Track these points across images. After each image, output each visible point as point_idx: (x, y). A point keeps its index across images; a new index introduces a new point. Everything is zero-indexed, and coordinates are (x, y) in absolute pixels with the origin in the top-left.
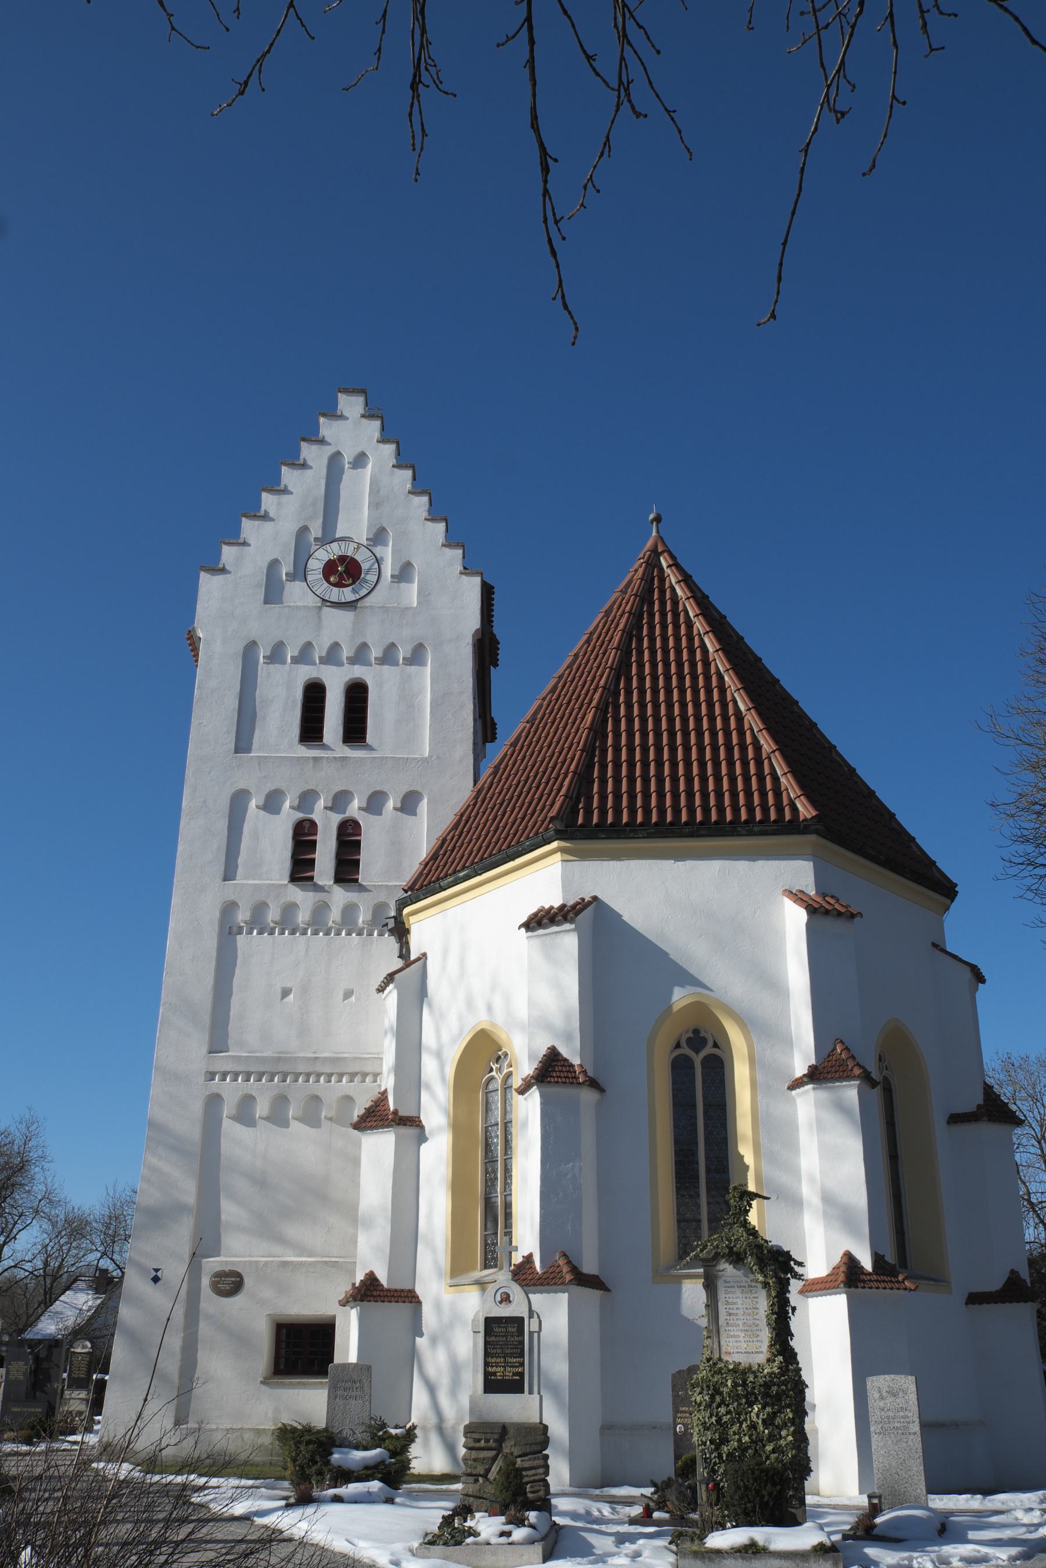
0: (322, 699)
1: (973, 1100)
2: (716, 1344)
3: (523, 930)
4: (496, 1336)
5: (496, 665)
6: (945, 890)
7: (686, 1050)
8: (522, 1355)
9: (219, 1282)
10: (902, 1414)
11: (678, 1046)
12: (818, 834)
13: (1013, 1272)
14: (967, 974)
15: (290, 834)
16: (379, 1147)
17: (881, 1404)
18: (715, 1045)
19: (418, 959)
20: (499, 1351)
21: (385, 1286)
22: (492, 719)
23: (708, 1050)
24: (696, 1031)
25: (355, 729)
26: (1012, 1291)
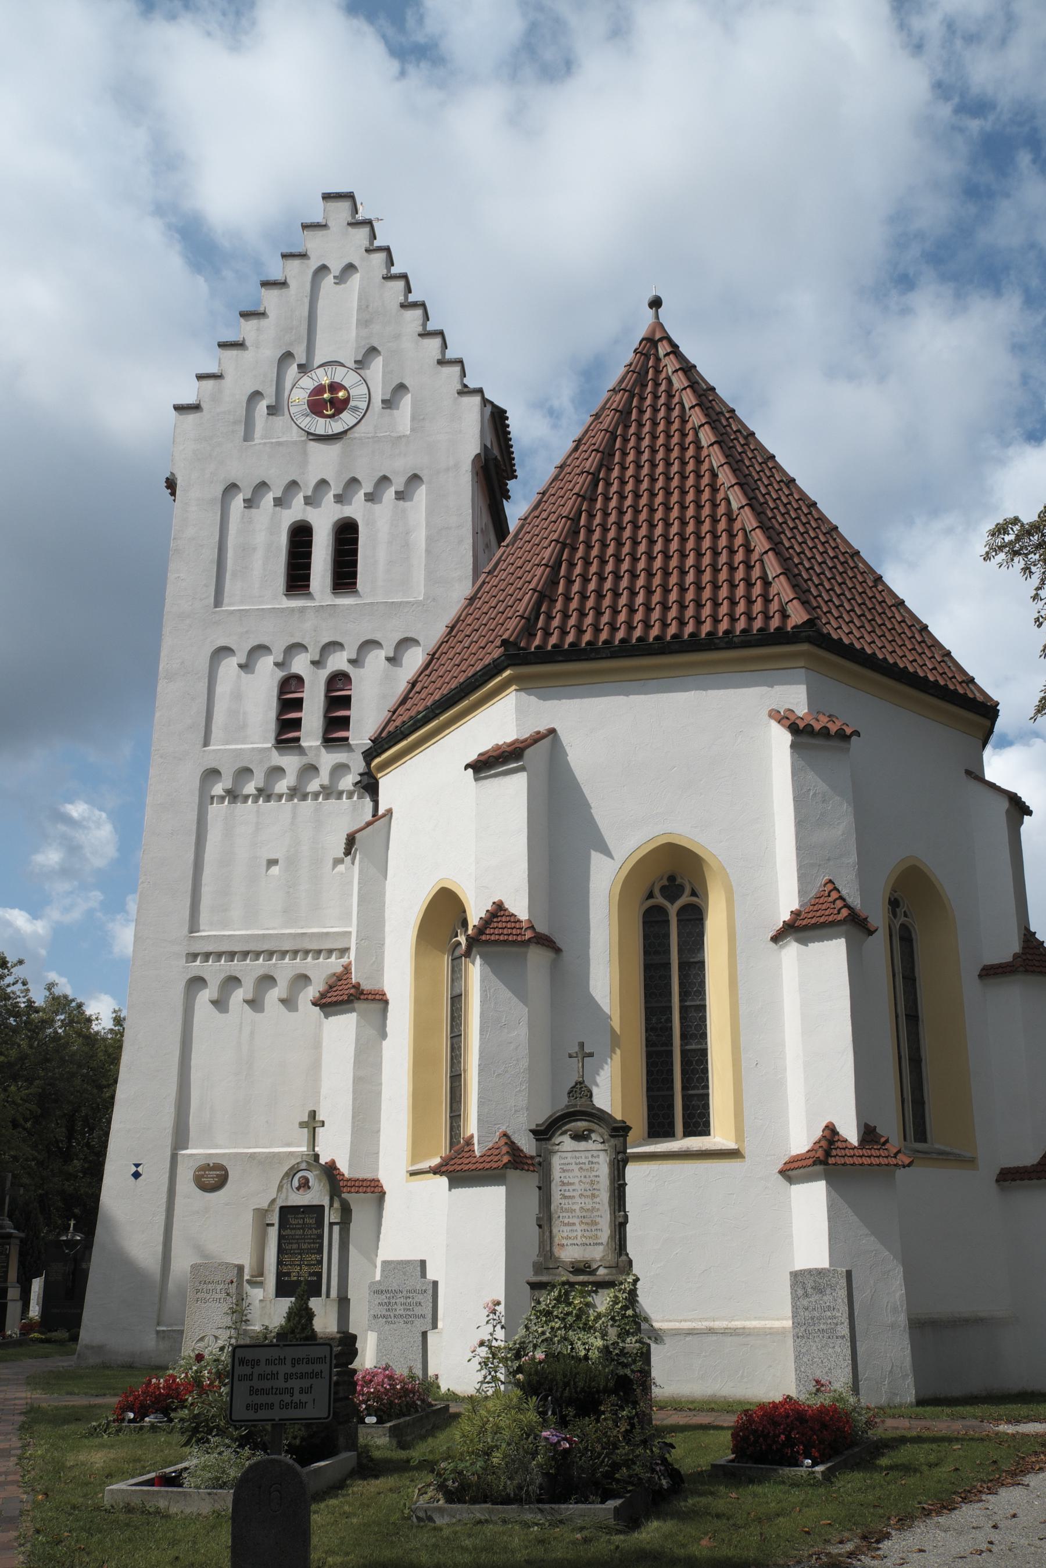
1: (1008, 948)
2: (547, 1234)
3: (470, 771)
4: (291, 1229)
7: (660, 900)
8: (320, 1251)
9: (202, 1176)
10: (829, 1314)
11: (651, 895)
12: (810, 642)
15: (275, 692)
16: (343, 1028)
17: (805, 1302)
18: (694, 893)
19: (384, 816)
20: (295, 1246)
21: (347, 1175)
23: (685, 899)
24: (672, 878)
25: (345, 576)
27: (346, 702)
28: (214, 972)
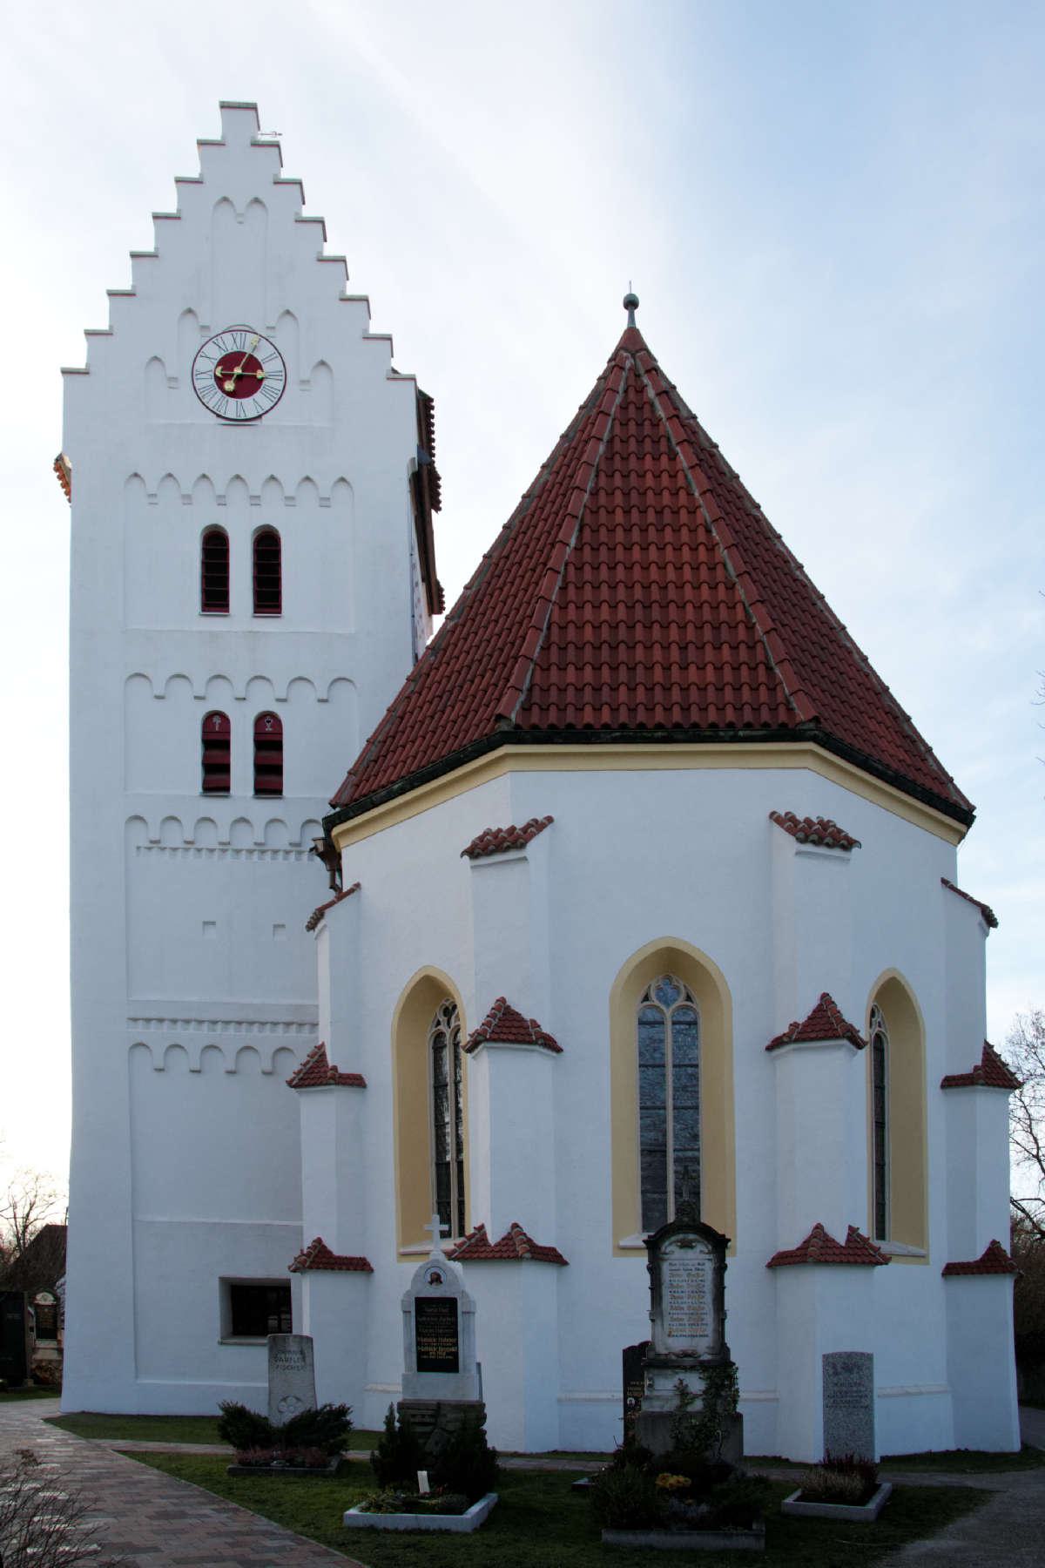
0: (224, 553)
1: (969, 1062)
3: (466, 858)
5: (438, 509)
6: (961, 814)
11: (646, 998)
13: (994, 1243)
14: (979, 917)
22: (438, 583)
26: (992, 1262)
27: (277, 746)
28: (158, 1037)
